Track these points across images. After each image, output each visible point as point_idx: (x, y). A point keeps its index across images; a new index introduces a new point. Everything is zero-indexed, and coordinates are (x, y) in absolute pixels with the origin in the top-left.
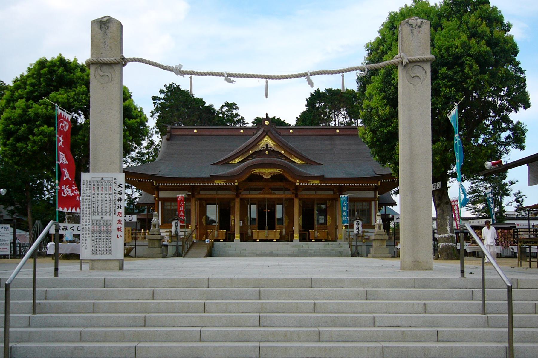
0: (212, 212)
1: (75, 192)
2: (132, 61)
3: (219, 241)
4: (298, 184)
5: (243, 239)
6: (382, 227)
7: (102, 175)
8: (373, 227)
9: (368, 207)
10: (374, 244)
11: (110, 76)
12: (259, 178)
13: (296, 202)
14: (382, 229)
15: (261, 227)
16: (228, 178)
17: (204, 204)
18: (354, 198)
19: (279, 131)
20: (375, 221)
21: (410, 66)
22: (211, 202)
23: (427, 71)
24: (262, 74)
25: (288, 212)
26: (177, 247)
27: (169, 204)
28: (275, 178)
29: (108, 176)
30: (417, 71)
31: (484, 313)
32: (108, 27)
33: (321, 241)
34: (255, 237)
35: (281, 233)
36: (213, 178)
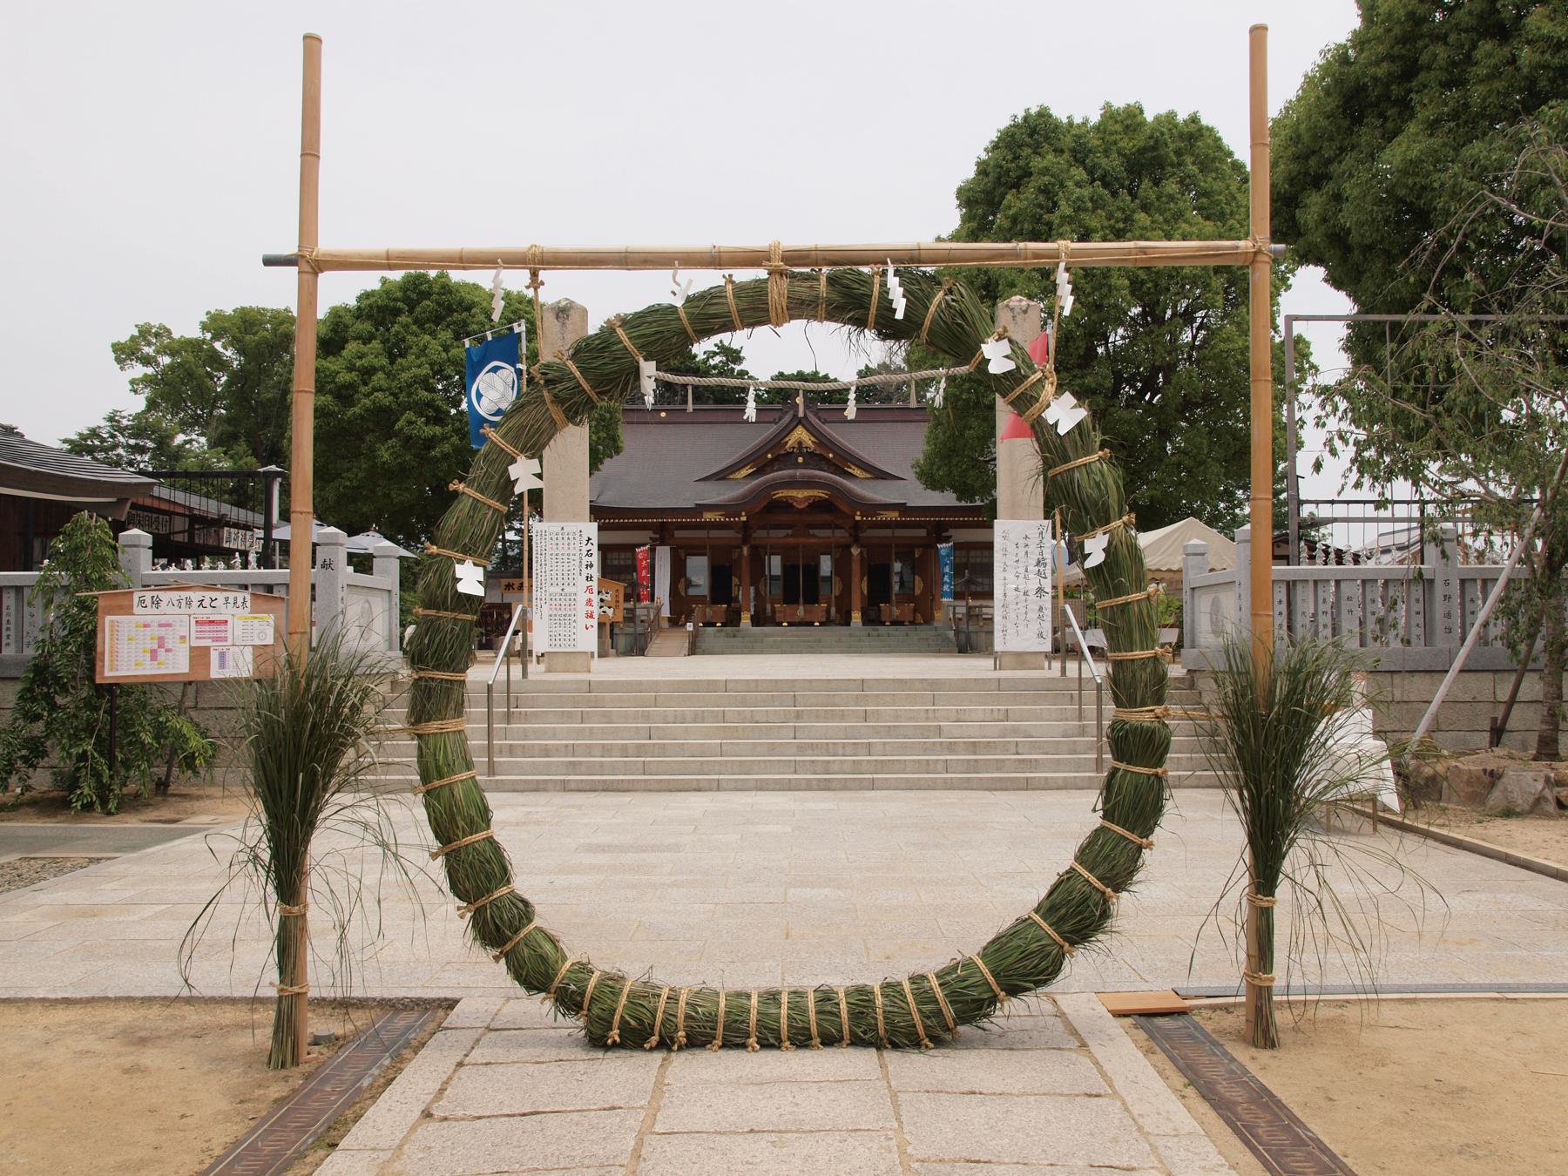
0: (699, 570)
3: (714, 625)
5: (757, 621)
13: (762, 274)
15: (790, 598)
16: (727, 508)
19: (823, 415)
22: (697, 550)
25: (841, 567)
27: (615, 555)
28: (816, 506)
29: (571, 527)
33: (901, 623)
34: (779, 617)
35: (828, 611)
36: (701, 509)
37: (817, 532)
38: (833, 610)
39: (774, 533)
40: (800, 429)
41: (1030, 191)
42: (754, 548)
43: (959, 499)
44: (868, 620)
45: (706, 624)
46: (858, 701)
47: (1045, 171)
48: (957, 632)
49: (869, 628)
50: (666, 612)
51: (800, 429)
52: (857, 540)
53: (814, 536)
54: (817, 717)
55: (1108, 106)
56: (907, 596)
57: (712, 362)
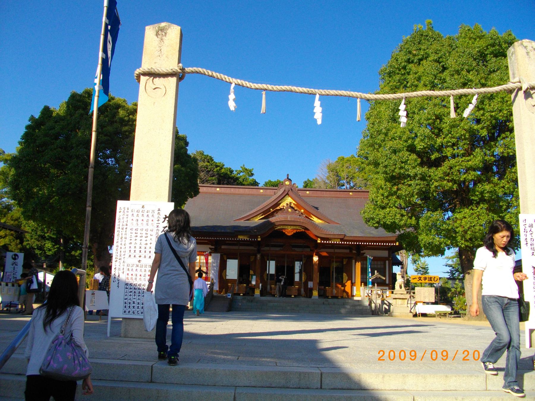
3: (239, 294)
4: (319, 241)
9: (382, 266)
12: (280, 234)
17: (225, 258)
18: (379, 257)
32: (166, 34)
38: (302, 290)
39: (272, 249)
49: (323, 300)
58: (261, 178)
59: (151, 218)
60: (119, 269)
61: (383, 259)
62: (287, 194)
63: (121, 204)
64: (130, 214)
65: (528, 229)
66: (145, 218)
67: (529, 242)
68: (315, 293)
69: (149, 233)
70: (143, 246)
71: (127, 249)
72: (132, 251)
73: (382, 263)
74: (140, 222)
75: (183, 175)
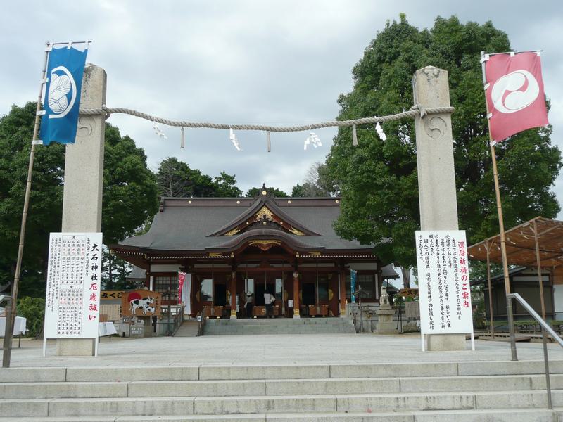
0: (207, 287)
1: (150, 308)
2: (116, 112)
3: (215, 317)
4: (297, 256)
5: (239, 315)
6: (387, 300)
7: (73, 234)
8: (378, 301)
10: (379, 320)
11: (90, 129)
12: (256, 249)
14: (388, 303)
19: (277, 202)
20: (380, 295)
21: (429, 118)
23: (447, 123)
24: (264, 125)
26: (169, 324)
27: (161, 278)
28: (274, 250)
29: (81, 236)
30: (436, 123)
31: (551, 406)
32: (89, 75)
36: (208, 251)
37: (275, 265)
38: (283, 309)
39: (250, 266)
40: (264, 209)
41: (398, 62)
42: (238, 275)
43: (362, 244)
44: (302, 315)
45: (211, 317)
46: (327, 388)
47: (407, 51)
48: (355, 321)
49: (305, 320)
50: (188, 311)
51: (264, 209)
52: (297, 270)
53: (272, 267)
54: (288, 406)
55: (439, 19)
56: (325, 301)
57: (219, 183)
58: (244, 188)
59: (81, 248)
60: (53, 295)
61: (372, 273)
62: (264, 205)
63: (53, 236)
64: (62, 244)
65: (424, 244)
66: (76, 248)
67: (424, 256)
68: (297, 311)
69: (80, 260)
70: (75, 273)
71: (60, 277)
72: (65, 278)
73: (371, 276)
74: (71, 251)
75: (139, 193)
